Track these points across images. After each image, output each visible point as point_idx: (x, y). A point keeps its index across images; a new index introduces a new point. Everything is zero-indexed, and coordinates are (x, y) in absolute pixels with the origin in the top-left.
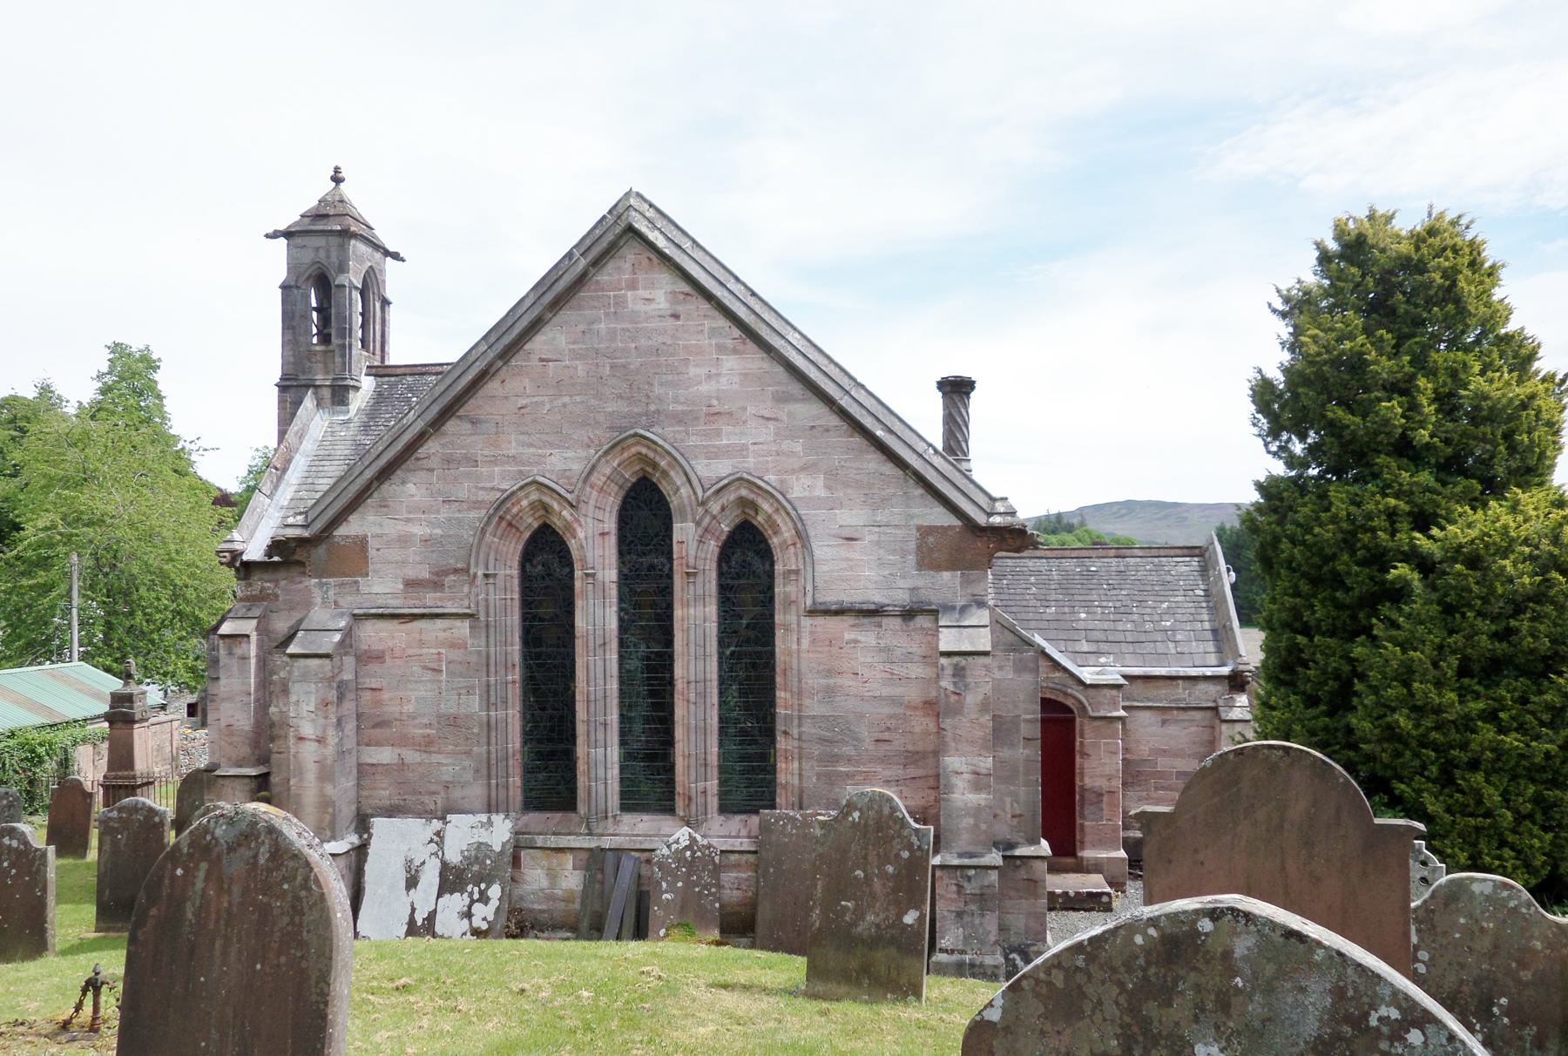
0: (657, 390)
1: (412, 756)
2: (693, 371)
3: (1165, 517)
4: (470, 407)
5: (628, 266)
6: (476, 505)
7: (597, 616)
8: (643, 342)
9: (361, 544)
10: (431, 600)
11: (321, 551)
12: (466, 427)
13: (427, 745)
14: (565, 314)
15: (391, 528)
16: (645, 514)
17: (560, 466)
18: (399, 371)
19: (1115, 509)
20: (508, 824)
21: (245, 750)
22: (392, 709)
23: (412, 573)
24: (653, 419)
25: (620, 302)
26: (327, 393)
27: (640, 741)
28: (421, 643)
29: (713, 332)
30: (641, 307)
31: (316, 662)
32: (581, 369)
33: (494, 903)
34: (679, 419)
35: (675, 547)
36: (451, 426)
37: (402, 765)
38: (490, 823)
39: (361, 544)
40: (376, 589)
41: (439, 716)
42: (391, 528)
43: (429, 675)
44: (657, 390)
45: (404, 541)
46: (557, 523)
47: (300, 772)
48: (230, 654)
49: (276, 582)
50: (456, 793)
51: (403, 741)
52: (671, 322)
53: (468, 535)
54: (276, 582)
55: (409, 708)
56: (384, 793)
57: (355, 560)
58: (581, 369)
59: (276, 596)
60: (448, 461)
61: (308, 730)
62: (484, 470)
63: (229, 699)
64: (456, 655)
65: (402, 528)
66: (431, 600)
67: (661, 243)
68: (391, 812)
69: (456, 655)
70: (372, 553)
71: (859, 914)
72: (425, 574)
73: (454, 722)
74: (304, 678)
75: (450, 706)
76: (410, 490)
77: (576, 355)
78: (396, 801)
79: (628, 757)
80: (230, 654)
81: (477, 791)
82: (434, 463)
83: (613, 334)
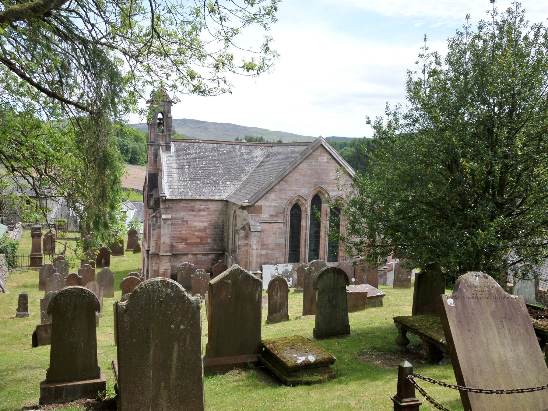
0: (324, 177)
1: (269, 252)
2: (331, 174)
3: (200, 127)
4: (286, 179)
5: (319, 152)
6: (286, 199)
7: (306, 222)
8: (321, 168)
9: (261, 207)
10: (275, 219)
11: (252, 208)
12: (285, 183)
13: (273, 250)
14: (307, 161)
15: (267, 204)
16: (317, 200)
17: (303, 192)
18: (179, 141)
19: (179, 122)
20: (292, 266)
21: (168, 249)
22: (266, 242)
23: (271, 213)
24: (322, 183)
25: (317, 159)
26: (164, 148)
27: (313, 247)
28: (273, 228)
29: (335, 166)
30: (322, 160)
31: (257, 233)
32: (309, 172)
33: (291, 282)
34: (327, 183)
35: (322, 208)
36: (281, 182)
37: (267, 254)
38: (287, 265)
39: (261, 207)
40: (264, 217)
41: (276, 243)
42: (267, 204)
43: (274, 235)
44: (324, 177)
45: (270, 206)
46: (300, 203)
47: (252, 256)
48: (165, 223)
49: (173, 205)
50: (278, 260)
51: (268, 249)
52: (327, 164)
53: (284, 206)
54: (173, 205)
55: (269, 242)
56: (263, 260)
57: (259, 210)
58: (309, 172)
59: (173, 208)
60: (280, 190)
61: (254, 247)
62: (287, 192)
63: (164, 235)
64: (280, 231)
65: (269, 204)
66: (275, 219)
67: (327, 148)
68: (265, 264)
69: (280, 231)
70: (263, 209)
71: (402, 277)
72: (274, 214)
73: (279, 245)
74: (254, 236)
75: (278, 241)
76: (272, 196)
77: (308, 169)
78: (266, 261)
79: (310, 251)
80: (165, 223)
81: (283, 259)
82: (277, 190)
83: (315, 165)
